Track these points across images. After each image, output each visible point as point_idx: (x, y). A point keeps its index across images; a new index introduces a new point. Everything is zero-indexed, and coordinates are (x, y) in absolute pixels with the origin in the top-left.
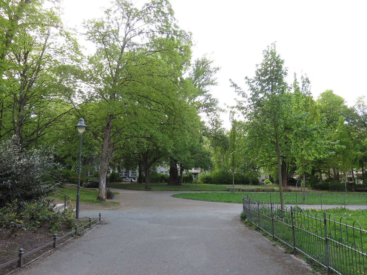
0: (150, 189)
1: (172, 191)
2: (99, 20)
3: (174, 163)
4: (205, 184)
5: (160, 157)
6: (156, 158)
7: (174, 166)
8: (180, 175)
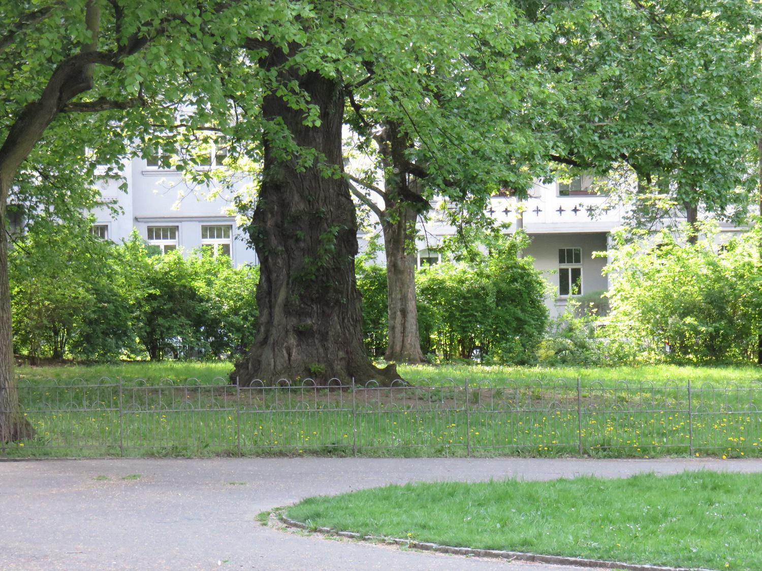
0: (15, 437)
1: (294, 454)
2: (402, 399)
3: (314, 118)
4: (688, 372)
5: (136, 44)
6: (90, 56)
7: (308, 156)
8: (382, 261)
